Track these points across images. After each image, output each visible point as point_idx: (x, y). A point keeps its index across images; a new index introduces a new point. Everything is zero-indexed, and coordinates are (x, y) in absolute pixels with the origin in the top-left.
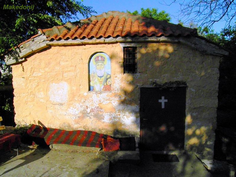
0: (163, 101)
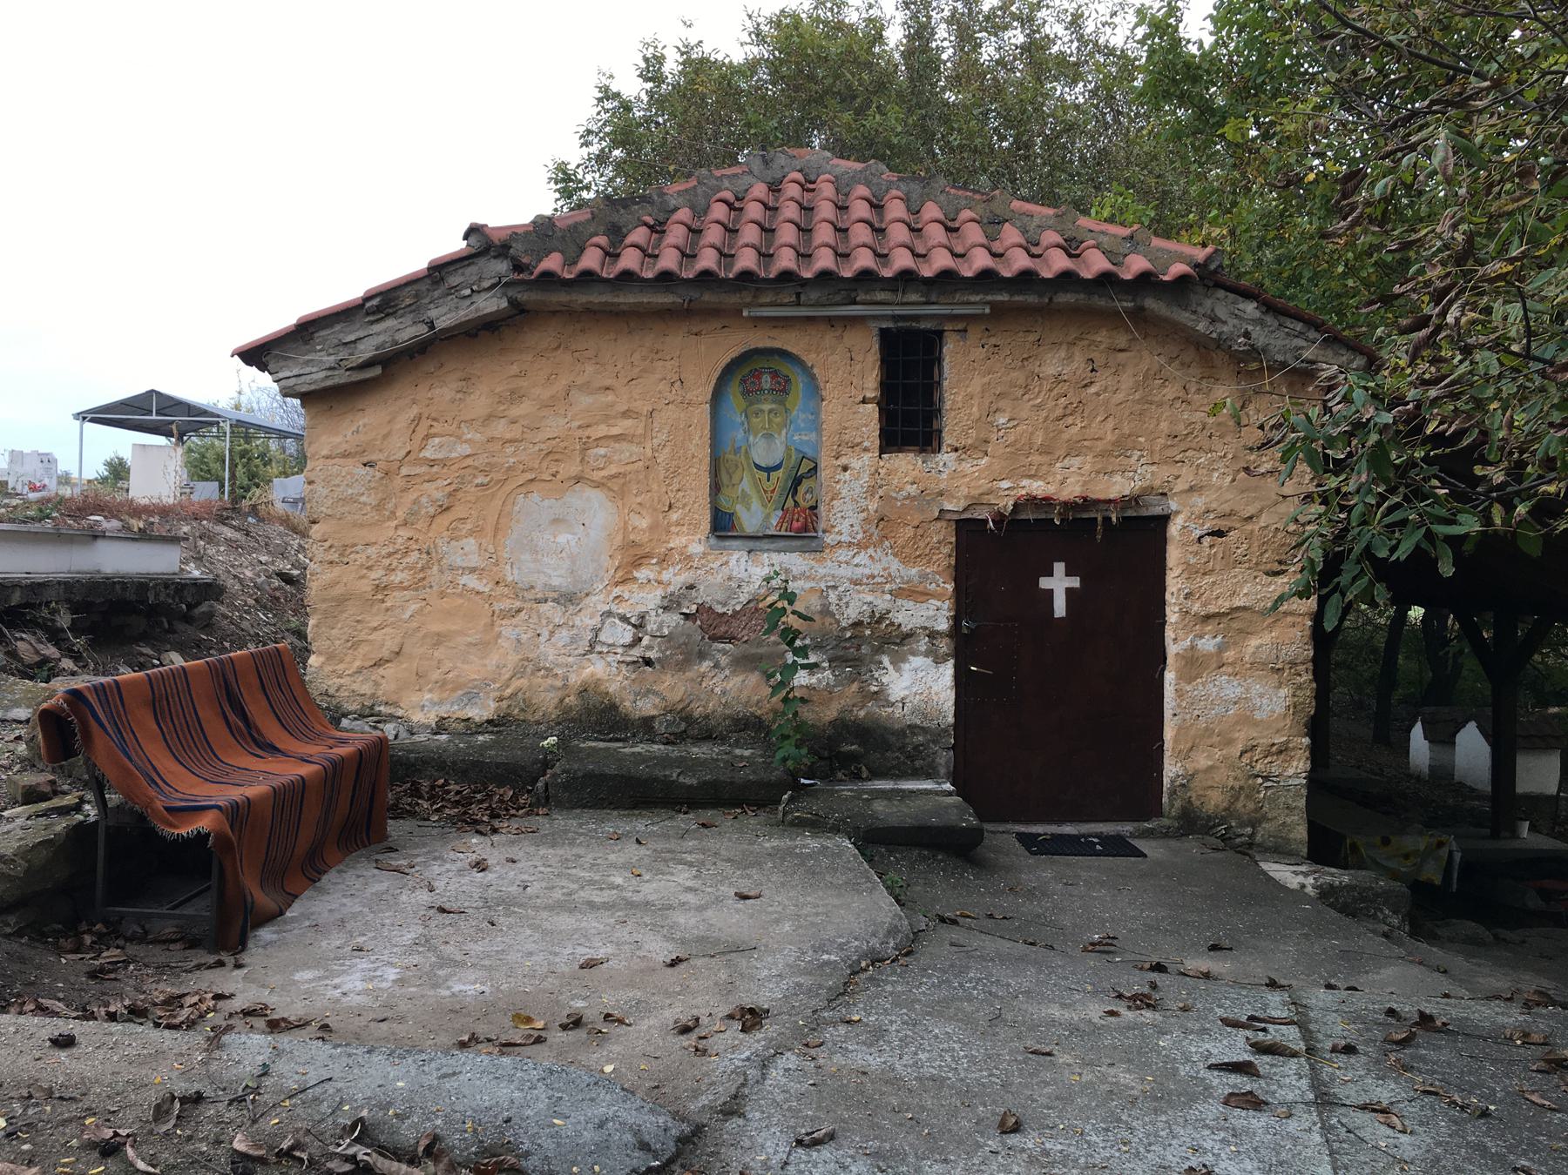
0: (1059, 583)
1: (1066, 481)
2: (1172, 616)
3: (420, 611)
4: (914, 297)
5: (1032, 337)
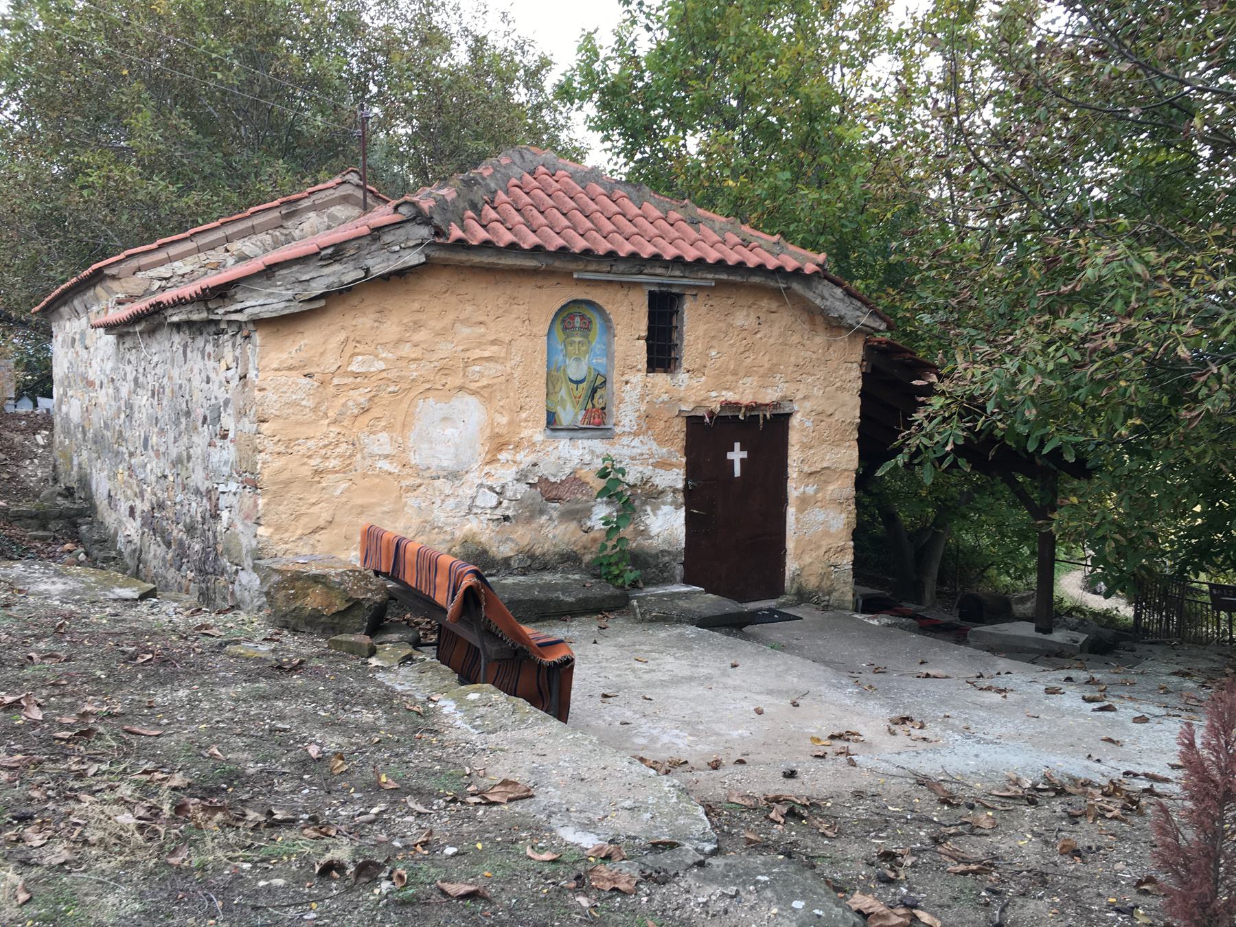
0: (737, 455)
1: (745, 392)
2: (793, 473)
3: (348, 489)
4: (678, 273)
5: (730, 302)
